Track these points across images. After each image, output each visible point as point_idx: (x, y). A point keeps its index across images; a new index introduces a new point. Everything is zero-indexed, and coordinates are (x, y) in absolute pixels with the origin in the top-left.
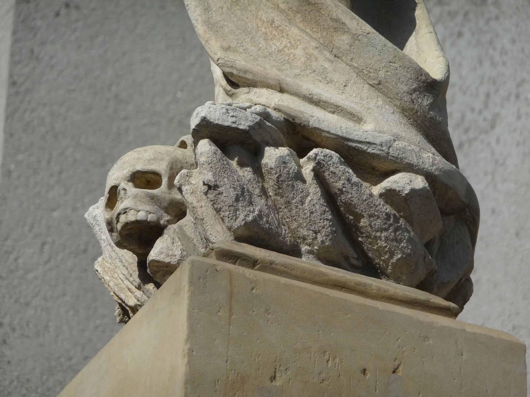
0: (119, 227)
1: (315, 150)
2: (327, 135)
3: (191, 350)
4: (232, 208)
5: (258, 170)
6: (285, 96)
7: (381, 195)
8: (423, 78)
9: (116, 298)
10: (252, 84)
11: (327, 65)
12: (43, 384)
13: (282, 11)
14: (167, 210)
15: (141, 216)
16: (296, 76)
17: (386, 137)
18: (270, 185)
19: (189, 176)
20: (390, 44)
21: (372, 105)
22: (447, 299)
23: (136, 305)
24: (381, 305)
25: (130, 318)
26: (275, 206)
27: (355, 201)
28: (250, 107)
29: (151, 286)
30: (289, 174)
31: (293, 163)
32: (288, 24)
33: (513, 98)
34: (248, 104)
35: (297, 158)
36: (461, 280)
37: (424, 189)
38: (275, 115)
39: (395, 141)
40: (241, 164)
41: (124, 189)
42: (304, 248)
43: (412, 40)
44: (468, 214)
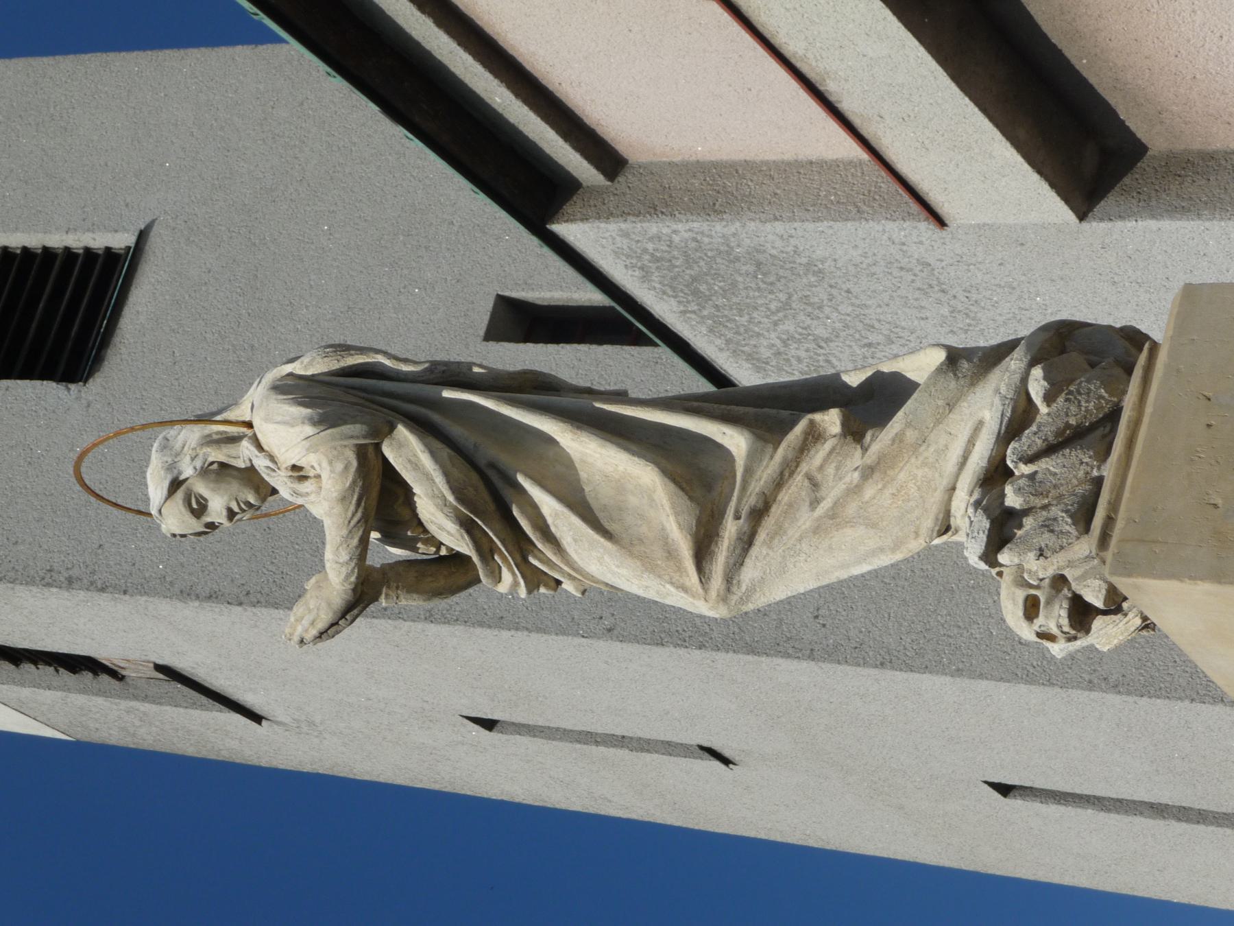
0: (1073, 632)
1: (1009, 463)
2: (994, 451)
3: (1191, 578)
4: (1060, 536)
5: (1026, 512)
6: (959, 485)
7: (1049, 406)
8: (944, 367)
9: (1133, 634)
10: (948, 514)
11: (932, 449)
12: (1143, 647)
13: (884, 487)
14: (1059, 591)
15: (1064, 613)
16: (941, 476)
17: (997, 401)
18: (1038, 502)
19: (1030, 572)
20: (915, 396)
21: (967, 411)
22: (1140, 350)
23: (1141, 618)
24: (1149, 409)
25: (1152, 623)
26: (1057, 497)
27: (1053, 428)
28: (969, 517)
29: (1125, 605)
30: (1029, 486)
31: (1020, 481)
32: (895, 482)
33: (905, 248)
34: (967, 519)
35: (1014, 477)
36: (1122, 337)
37: (1043, 369)
38: (976, 496)
39: (1000, 393)
40: (1020, 526)
41: (1040, 626)
42: (1095, 473)
43: (910, 375)
44: (1064, 330)
